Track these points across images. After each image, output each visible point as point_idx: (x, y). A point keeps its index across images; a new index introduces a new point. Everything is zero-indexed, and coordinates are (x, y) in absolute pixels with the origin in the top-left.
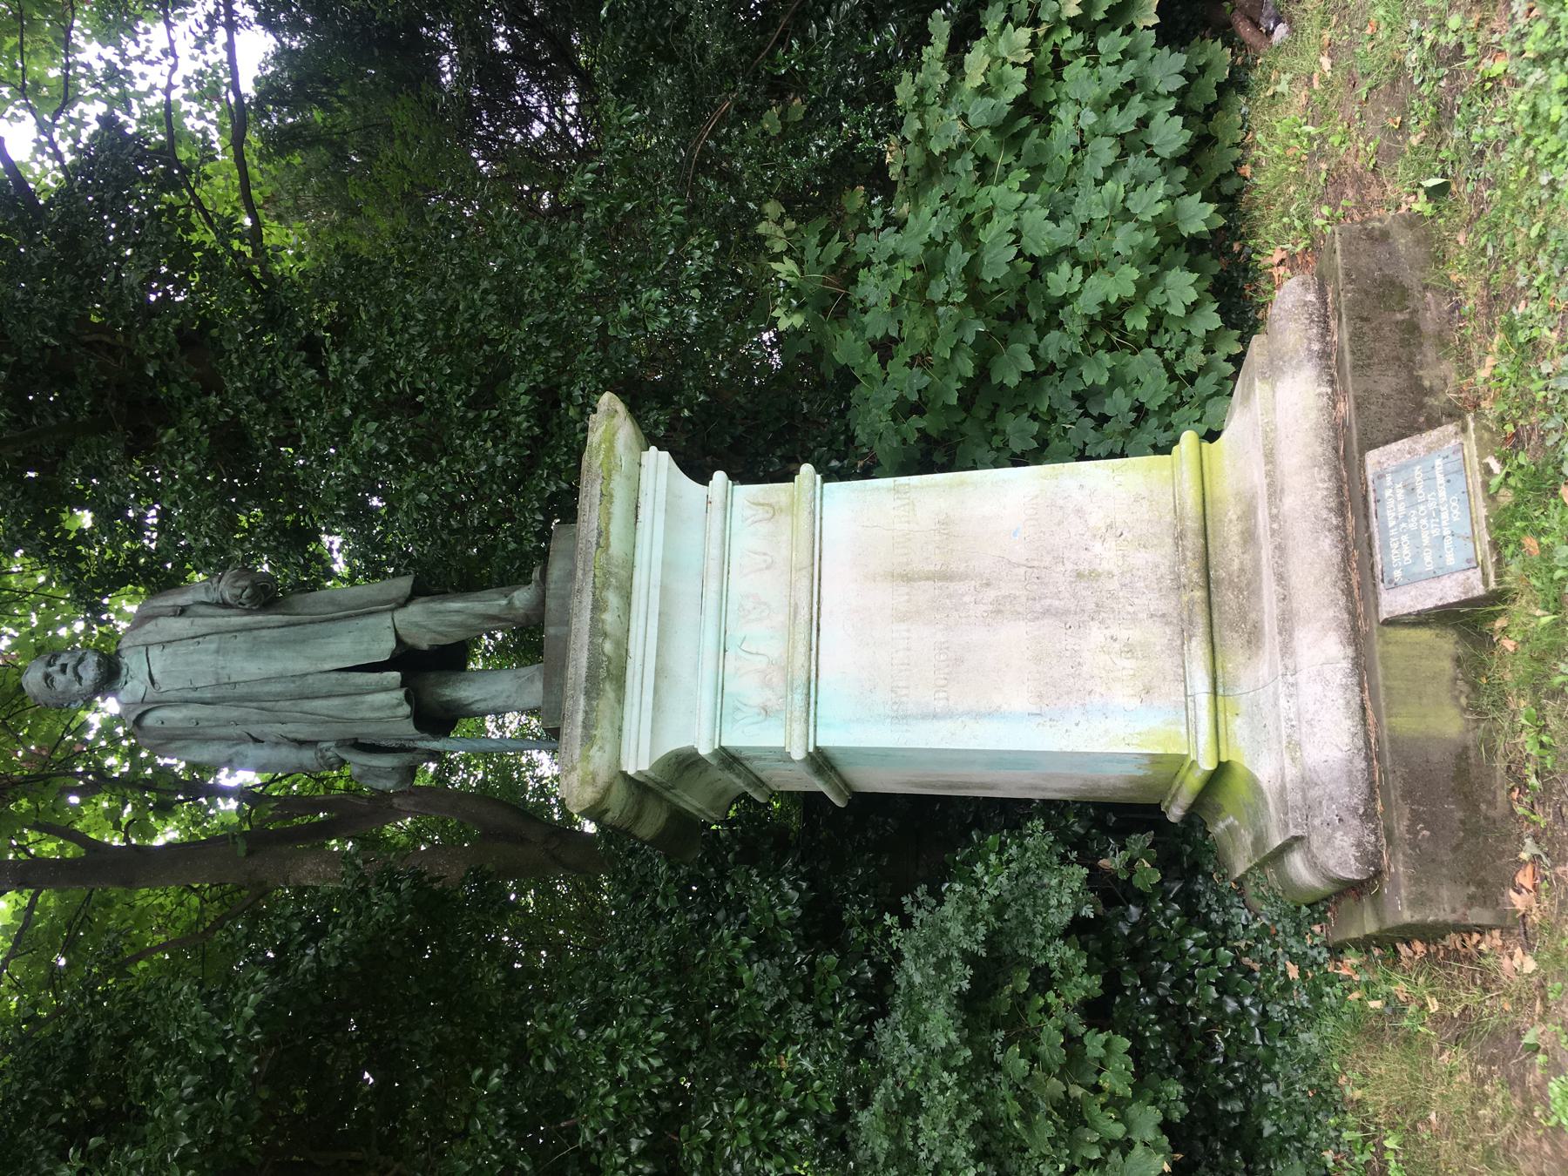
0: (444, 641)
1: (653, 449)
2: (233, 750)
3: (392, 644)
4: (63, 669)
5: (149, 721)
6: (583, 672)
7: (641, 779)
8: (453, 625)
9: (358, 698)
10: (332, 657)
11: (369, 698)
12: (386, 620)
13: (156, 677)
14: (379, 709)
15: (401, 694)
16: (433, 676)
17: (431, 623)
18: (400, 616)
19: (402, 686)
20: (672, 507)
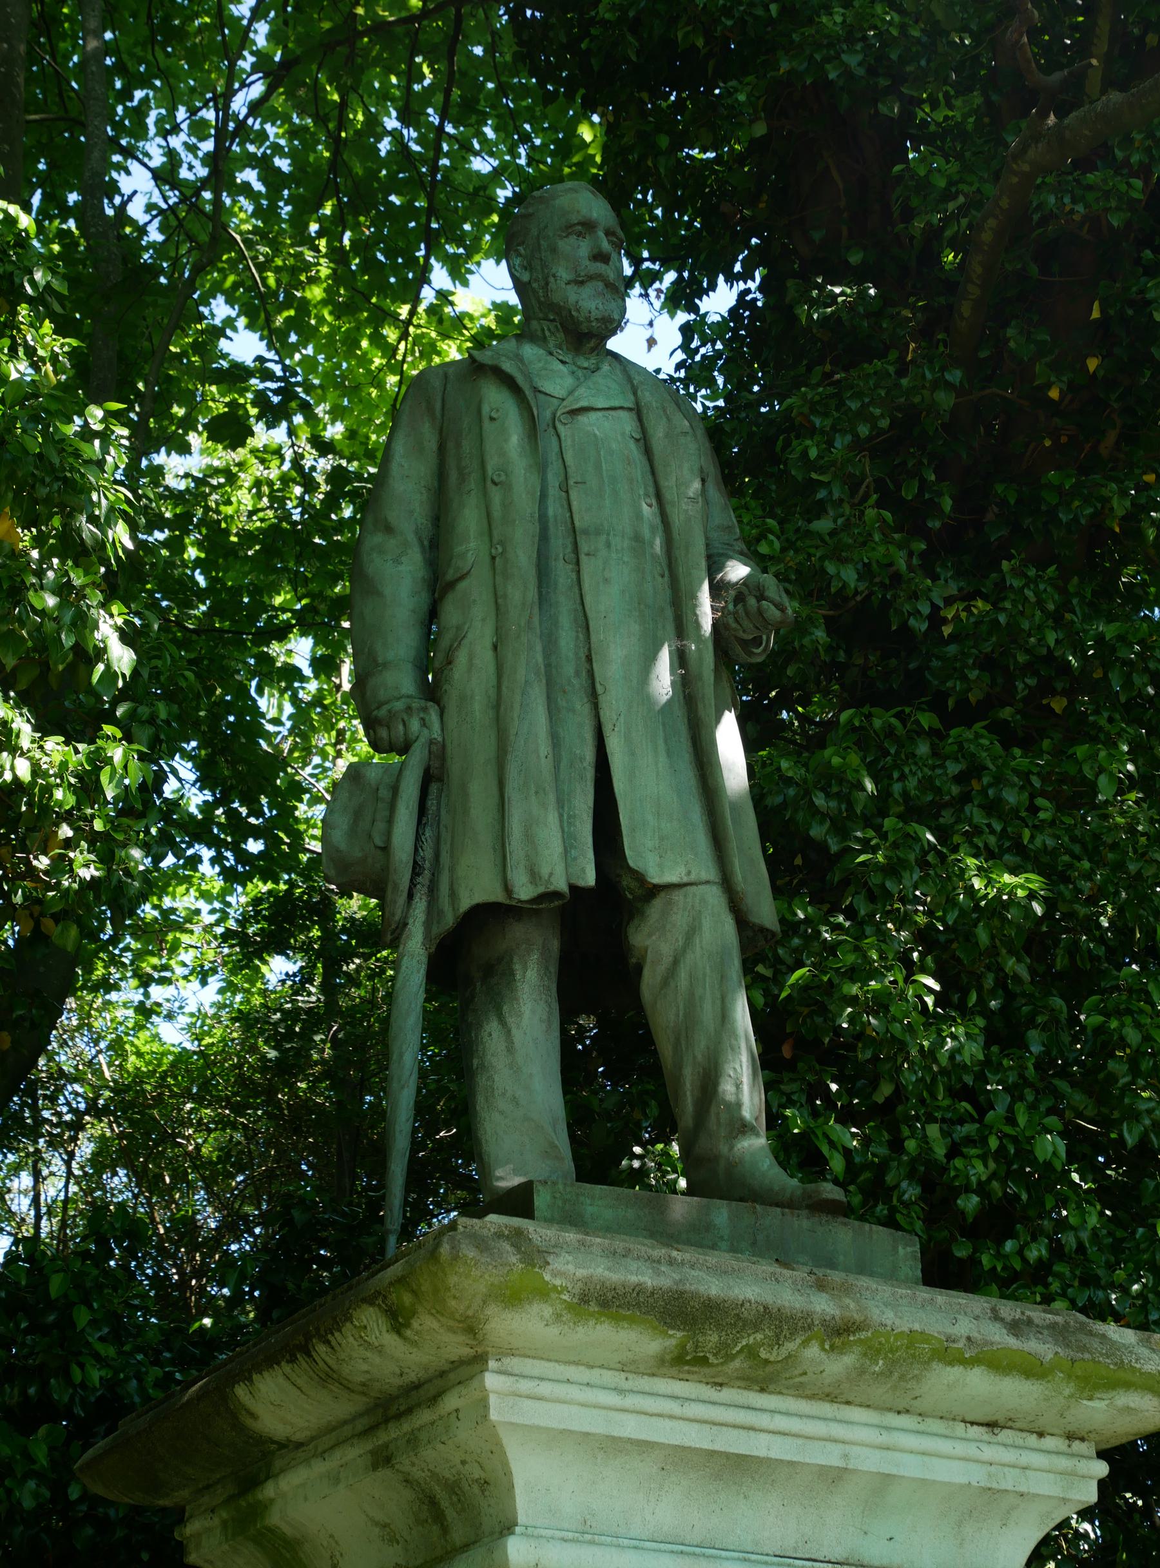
0: (650, 979)
1: (1102, 1469)
2: (411, 537)
3: (656, 877)
4: (601, 257)
5: (494, 397)
6: (713, 1288)
7: (451, 1402)
8: (692, 1004)
9: (552, 797)
10: (633, 754)
11: (552, 818)
12: (706, 870)
13: (583, 419)
14: (529, 837)
15: (561, 885)
16: (555, 945)
17: (698, 957)
18: (714, 897)
19: (573, 888)
20: (989, 1503)
